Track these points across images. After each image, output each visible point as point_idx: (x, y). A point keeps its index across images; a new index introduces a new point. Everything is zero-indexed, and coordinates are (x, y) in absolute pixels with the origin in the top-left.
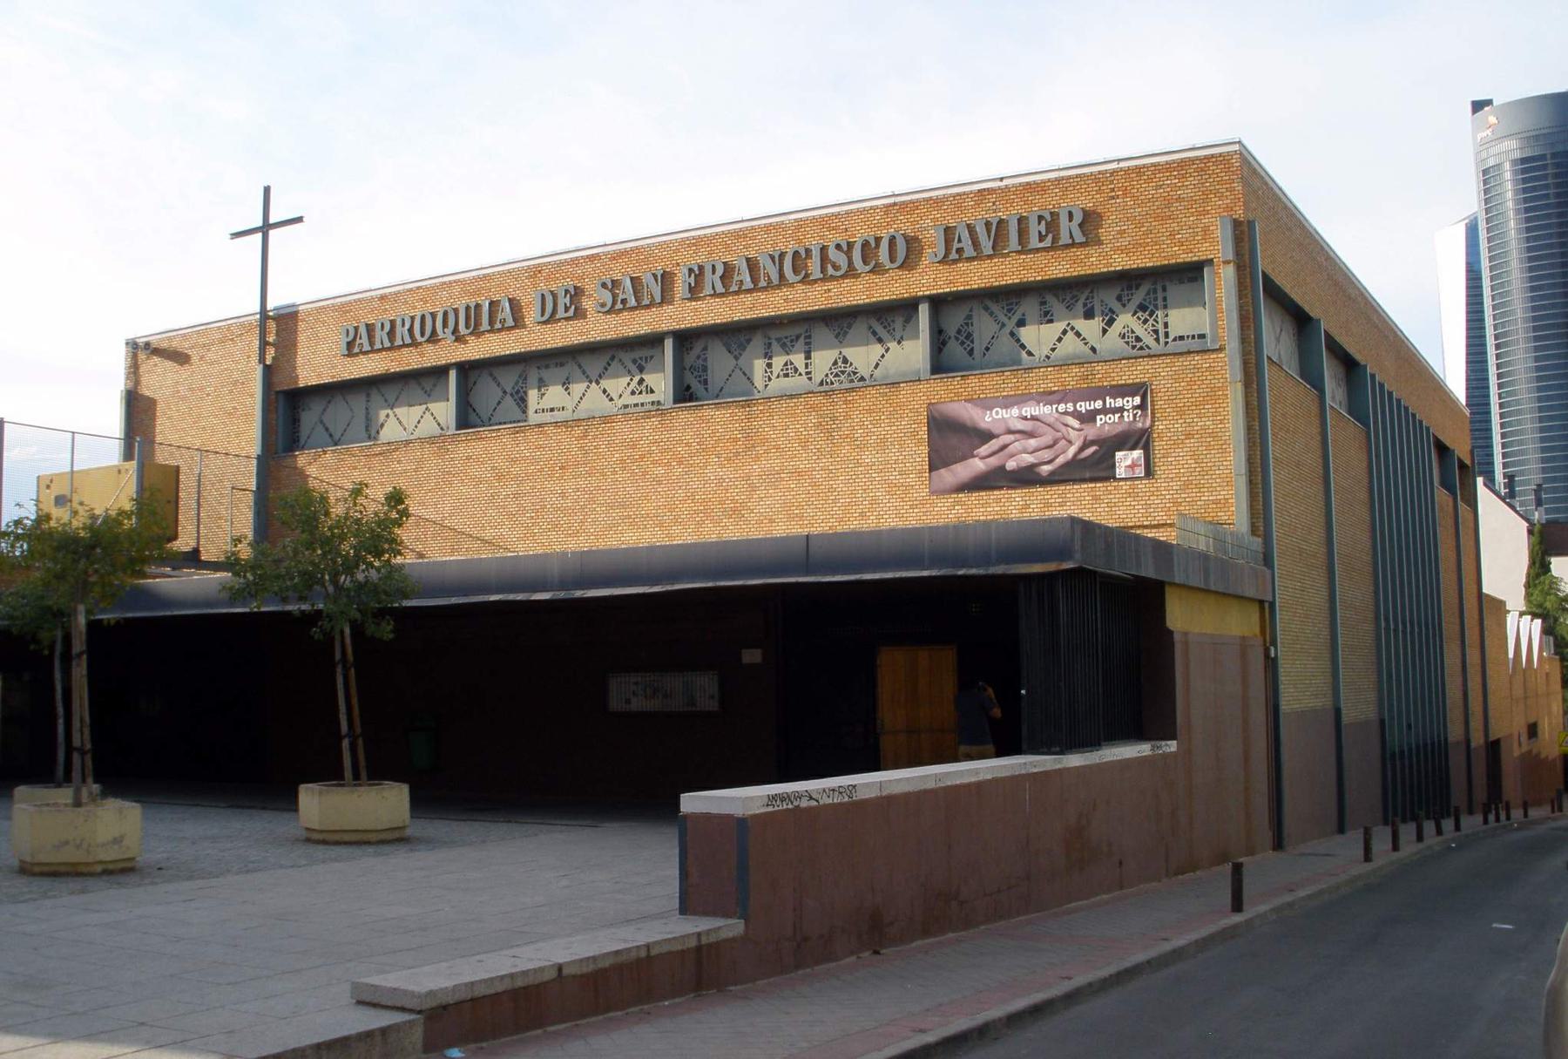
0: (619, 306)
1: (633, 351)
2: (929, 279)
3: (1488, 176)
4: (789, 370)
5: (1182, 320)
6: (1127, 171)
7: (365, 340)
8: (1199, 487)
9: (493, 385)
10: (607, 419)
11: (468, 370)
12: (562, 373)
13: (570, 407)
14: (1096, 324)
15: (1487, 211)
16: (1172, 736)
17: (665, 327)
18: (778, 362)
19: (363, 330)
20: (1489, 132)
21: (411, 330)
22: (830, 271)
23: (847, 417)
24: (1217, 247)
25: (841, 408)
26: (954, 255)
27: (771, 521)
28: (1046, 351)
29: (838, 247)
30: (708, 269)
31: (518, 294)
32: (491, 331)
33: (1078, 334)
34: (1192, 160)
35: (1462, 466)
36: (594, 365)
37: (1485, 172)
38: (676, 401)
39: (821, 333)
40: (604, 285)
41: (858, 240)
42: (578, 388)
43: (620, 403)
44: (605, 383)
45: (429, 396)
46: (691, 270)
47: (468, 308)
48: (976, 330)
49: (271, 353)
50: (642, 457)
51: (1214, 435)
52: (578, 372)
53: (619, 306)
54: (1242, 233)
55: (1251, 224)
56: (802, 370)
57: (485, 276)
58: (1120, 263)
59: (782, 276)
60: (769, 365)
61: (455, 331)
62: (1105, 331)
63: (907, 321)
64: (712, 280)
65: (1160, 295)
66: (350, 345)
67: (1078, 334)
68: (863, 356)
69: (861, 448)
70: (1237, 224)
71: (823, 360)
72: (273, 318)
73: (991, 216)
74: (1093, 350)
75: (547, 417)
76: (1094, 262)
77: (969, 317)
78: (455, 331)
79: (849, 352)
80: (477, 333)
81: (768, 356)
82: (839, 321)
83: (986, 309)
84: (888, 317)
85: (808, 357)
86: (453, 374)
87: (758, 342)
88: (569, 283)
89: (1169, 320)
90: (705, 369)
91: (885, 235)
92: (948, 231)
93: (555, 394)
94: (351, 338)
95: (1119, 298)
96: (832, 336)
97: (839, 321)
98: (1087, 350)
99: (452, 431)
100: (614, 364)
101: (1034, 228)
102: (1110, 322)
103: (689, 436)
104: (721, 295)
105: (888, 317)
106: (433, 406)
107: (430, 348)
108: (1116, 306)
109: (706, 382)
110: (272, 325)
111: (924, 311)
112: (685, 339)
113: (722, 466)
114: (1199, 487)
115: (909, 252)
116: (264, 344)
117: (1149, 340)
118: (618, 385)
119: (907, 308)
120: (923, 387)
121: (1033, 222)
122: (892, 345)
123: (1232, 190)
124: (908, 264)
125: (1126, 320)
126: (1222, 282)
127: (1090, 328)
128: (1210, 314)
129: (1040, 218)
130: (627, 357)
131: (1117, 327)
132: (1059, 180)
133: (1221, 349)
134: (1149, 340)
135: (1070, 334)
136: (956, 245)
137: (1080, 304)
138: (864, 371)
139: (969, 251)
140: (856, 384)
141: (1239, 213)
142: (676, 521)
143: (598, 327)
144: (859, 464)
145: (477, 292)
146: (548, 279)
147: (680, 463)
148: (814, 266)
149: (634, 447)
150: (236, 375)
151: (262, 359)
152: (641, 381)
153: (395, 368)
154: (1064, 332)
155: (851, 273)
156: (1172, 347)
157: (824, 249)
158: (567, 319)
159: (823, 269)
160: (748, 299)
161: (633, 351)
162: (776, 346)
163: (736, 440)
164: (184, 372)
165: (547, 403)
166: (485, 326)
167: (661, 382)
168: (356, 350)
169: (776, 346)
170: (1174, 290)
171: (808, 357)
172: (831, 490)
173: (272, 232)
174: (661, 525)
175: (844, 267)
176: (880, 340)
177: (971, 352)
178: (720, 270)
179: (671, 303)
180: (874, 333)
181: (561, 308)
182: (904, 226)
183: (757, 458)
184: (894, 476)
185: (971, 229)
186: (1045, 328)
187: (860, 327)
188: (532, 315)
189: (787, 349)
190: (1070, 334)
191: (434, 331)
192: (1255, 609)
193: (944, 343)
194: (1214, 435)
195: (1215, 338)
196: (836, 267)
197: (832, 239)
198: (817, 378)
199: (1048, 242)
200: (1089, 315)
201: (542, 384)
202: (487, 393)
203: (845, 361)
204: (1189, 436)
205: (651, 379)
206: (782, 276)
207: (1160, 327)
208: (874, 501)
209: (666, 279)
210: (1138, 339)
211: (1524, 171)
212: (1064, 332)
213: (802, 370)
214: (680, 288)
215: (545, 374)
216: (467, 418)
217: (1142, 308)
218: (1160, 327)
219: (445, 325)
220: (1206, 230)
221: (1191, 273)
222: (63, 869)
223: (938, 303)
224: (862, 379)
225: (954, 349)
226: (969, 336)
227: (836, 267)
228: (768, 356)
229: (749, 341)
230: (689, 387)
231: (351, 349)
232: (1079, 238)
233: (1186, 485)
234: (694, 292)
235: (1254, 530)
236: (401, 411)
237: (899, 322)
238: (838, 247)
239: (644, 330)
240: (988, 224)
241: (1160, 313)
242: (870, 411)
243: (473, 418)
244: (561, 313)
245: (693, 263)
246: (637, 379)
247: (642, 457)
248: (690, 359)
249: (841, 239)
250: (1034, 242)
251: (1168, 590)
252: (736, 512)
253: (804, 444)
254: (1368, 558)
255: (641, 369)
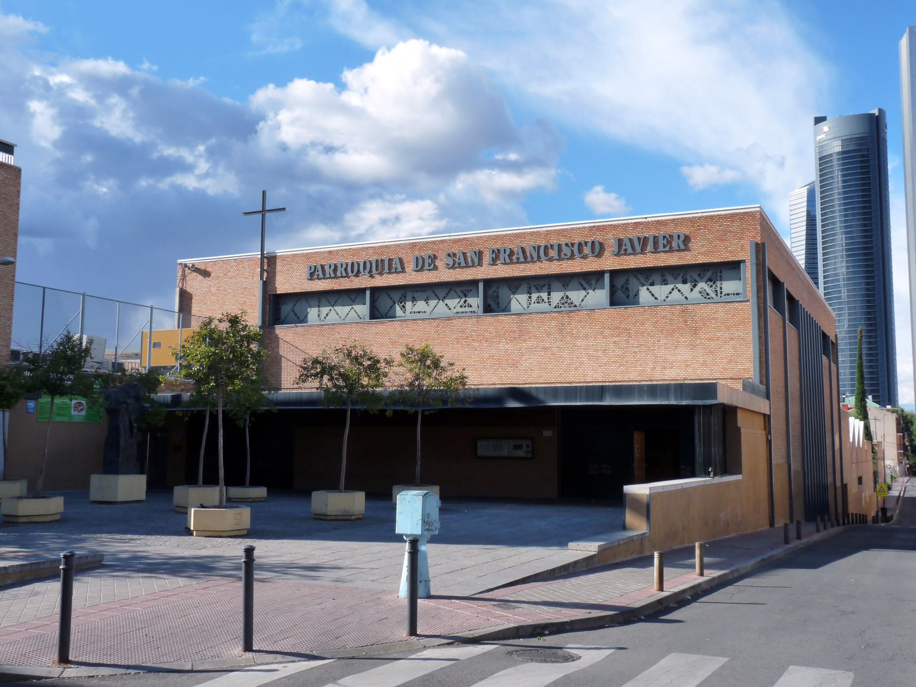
0: (457, 265)
1: (464, 288)
2: (609, 262)
3: (824, 162)
4: (540, 300)
5: (729, 286)
6: (707, 217)
7: (320, 273)
8: (736, 362)
9: (388, 299)
10: (449, 319)
11: (375, 290)
12: (425, 295)
13: (428, 311)
14: (688, 286)
15: (821, 181)
16: (741, 473)
17: (480, 276)
18: (535, 296)
19: (319, 268)
20: (824, 136)
21: (346, 270)
22: (563, 256)
23: (569, 324)
24: (746, 255)
25: (566, 320)
26: (622, 252)
27: (532, 370)
28: (664, 297)
29: (567, 245)
30: (502, 251)
31: (403, 256)
32: (389, 273)
33: (679, 291)
34: (737, 214)
35: (833, 343)
36: (441, 293)
37: (821, 159)
38: (484, 312)
39: (555, 284)
40: (449, 255)
41: (576, 241)
42: (433, 303)
43: (455, 311)
44: (447, 301)
45: (353, 302)
46: (493, 251)
47: (377, 261)
48: (630, 286)
49: (265, 275)
50: (467, 338)
51: (743, 339)
52: (432, 293)
53: (457, 265)
54: (760, 249)
55: (763, 244)
56: (546, 300)
57: (386, 246)
58: (702, 260)
59: (539, 257)
60: (530, 297)
61: (370, 272)
62: (692, 290)
63: (598, 281)
64: (487, 258)
65: (719, 275)
66: (312, 274)
67: (679, 291)
68: (576, 296)
69: (576, 338)
70: (757, 244)
71: (556, 296)
72: (267, 258)
73: (640, 235)
74: (686, 298)
75: (417, 316)
76: (688, 258)
77: (628, 280)
78: (370, 272)
79: (569, 294)
80: (381, 274)
81: (529, 293)
82: (565, 280)
83: (636, 277)
84: (589, 279)
85: (549, 294)
86: (368, 293)
87: (524, 287)
88: (430, 253)
89: (723, 286)
90: (498, 297)
91: (589, 240)
92: (620, 242)
93: (421, 305)
94: (313, 270)
95: (699, 275)
96: (560, 285)
97: (565, 280)
98: (683, 298)
99: (367, 320)
100: (452, 292)
101: (661, 242)
102: (695, 286)
103: (491, 329)
104: (508, 264)
105: (589, 279)
106: (356, 307)
107: (356, 279)
108: (698, 279)
109: (498, 303)
110: (266, 260)
111: (607, 277)
112: (488, 283)
113: (507, 343)
114: (736, 362)
115: (598, 250)
116: (262, 271)
117: (713, 295)
118: (453, 302)
119: (599, 275)
120: (606, 311)
121: (661, 239)
122: (591, 291)
123: (755, 229)
124: (599, 255)
125: (702, 285)
126: (749, 272)
127: (685, 288)
128: (743, 286)
129: (664, 237)
130: (458, 290)
131: (698, 288)
132: (673, 220)
133: (748, 301)
134: (713, 295)
135: (676, 290)
136: (624, 247)
137: (680, 277)
138: (576, 303)
139: (630, 251)
140: (573, 308)
141: (759, 240)
142: (484, 368)
143: (445, 275)
144: (574, 345)
145: (382, 254)
146: (420, 249)
147: (486, 341)
148: (553, 253)
149: (463, 332)
150: (245, 285)
151: (262, 278)
152: (465, 302)
153: (336, 287)
154: (673, 289)
155: (572, 257)
156: (724, 299)
157: (559, 245)
158: (429, 270)
159: (559, 255)
160: (522, 266)
161: (464, 288)
162: (533, 289)
163: (515, 332)
164: (206, 282)
165: (416, 309)
166: (386, 270)
167: (476, 302)
168: (315, 277)
169: (533, 289)
170: (725, 273)
171: (549, 294)
172: (561, 357)
173: (268, 215)
174: (476, 370)
175: (569, 254)
176: (584, 289)
177: (628, 297)
178: (508, 252)
179: (482, 266)
180: (582, 285)
181: (426, 265)
182: (598, 237)
183: (525, 340)
184: (591, 352)
185: (631, 240)
186: (663, 287)
187: (574, 283)
188: (410, 267)
189: (539, 290)
190: (676, 290)
191: (359, 271)
192: (762, 418)
193: (615, 292)
194: (743, 339)
195: (745, 296)
196: (565, 255)
197: (563, 241)
198: (554, 304)
199: (667, 248)
200: (684, 282)
201: (414, 300)
202: (384, 302)
203: (567, 297)
204: (732, 339)
205: (471, 300)
206: (539, 257)
207: (718, 289)
208: (582, 363)
209: (480, 254)
210: (708, 294)
211: (843, 159)
212: (673, 289)
213: (546, 300)
214: (487, 258)
215: (416, 295)
216: (375, 314)
217: (710, 280)
218: (718, 289)
219: (365, 268)
220: (742, 246)
221: (733, 267)
222: (340, 518)
223: (614, 273)
224: (575, 306)
225: (620, 294)
226: (627, 289)
227: (565, 255)
228: (529, 293)
229: (520, 286)
230: (489, 306)
231: (312, 277)
232: (682, 247)
233: (730, 362)
234: (494, 262)
235: (761, 382)
236: (338, 309)
237: (593, 282)
238: (567, 245)
239: (470, 278)
240: (639, 239)
241: (718, 283)
242: (580, 322)
243: (377, 314)
244: (426, 267)
245: (498, 246)
246: (463, 300)
247: (467, 338)
248: (490, 292)
249: (568, 241)
250: (661, 248)
251: (740, 416)
252: (514, 365)
253: (548, 334)
254: (798, 393)
255: (466, 296)
